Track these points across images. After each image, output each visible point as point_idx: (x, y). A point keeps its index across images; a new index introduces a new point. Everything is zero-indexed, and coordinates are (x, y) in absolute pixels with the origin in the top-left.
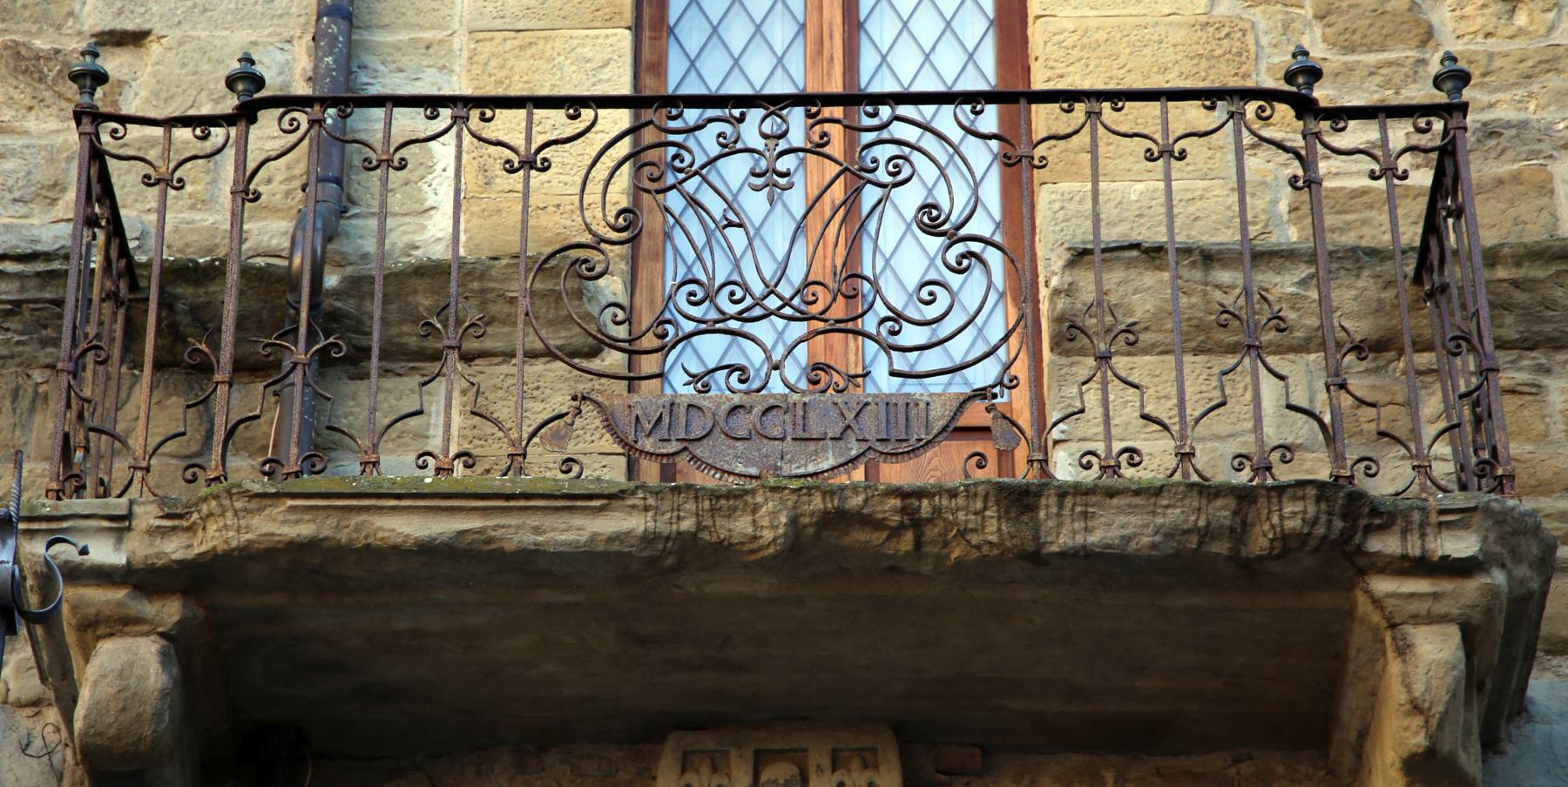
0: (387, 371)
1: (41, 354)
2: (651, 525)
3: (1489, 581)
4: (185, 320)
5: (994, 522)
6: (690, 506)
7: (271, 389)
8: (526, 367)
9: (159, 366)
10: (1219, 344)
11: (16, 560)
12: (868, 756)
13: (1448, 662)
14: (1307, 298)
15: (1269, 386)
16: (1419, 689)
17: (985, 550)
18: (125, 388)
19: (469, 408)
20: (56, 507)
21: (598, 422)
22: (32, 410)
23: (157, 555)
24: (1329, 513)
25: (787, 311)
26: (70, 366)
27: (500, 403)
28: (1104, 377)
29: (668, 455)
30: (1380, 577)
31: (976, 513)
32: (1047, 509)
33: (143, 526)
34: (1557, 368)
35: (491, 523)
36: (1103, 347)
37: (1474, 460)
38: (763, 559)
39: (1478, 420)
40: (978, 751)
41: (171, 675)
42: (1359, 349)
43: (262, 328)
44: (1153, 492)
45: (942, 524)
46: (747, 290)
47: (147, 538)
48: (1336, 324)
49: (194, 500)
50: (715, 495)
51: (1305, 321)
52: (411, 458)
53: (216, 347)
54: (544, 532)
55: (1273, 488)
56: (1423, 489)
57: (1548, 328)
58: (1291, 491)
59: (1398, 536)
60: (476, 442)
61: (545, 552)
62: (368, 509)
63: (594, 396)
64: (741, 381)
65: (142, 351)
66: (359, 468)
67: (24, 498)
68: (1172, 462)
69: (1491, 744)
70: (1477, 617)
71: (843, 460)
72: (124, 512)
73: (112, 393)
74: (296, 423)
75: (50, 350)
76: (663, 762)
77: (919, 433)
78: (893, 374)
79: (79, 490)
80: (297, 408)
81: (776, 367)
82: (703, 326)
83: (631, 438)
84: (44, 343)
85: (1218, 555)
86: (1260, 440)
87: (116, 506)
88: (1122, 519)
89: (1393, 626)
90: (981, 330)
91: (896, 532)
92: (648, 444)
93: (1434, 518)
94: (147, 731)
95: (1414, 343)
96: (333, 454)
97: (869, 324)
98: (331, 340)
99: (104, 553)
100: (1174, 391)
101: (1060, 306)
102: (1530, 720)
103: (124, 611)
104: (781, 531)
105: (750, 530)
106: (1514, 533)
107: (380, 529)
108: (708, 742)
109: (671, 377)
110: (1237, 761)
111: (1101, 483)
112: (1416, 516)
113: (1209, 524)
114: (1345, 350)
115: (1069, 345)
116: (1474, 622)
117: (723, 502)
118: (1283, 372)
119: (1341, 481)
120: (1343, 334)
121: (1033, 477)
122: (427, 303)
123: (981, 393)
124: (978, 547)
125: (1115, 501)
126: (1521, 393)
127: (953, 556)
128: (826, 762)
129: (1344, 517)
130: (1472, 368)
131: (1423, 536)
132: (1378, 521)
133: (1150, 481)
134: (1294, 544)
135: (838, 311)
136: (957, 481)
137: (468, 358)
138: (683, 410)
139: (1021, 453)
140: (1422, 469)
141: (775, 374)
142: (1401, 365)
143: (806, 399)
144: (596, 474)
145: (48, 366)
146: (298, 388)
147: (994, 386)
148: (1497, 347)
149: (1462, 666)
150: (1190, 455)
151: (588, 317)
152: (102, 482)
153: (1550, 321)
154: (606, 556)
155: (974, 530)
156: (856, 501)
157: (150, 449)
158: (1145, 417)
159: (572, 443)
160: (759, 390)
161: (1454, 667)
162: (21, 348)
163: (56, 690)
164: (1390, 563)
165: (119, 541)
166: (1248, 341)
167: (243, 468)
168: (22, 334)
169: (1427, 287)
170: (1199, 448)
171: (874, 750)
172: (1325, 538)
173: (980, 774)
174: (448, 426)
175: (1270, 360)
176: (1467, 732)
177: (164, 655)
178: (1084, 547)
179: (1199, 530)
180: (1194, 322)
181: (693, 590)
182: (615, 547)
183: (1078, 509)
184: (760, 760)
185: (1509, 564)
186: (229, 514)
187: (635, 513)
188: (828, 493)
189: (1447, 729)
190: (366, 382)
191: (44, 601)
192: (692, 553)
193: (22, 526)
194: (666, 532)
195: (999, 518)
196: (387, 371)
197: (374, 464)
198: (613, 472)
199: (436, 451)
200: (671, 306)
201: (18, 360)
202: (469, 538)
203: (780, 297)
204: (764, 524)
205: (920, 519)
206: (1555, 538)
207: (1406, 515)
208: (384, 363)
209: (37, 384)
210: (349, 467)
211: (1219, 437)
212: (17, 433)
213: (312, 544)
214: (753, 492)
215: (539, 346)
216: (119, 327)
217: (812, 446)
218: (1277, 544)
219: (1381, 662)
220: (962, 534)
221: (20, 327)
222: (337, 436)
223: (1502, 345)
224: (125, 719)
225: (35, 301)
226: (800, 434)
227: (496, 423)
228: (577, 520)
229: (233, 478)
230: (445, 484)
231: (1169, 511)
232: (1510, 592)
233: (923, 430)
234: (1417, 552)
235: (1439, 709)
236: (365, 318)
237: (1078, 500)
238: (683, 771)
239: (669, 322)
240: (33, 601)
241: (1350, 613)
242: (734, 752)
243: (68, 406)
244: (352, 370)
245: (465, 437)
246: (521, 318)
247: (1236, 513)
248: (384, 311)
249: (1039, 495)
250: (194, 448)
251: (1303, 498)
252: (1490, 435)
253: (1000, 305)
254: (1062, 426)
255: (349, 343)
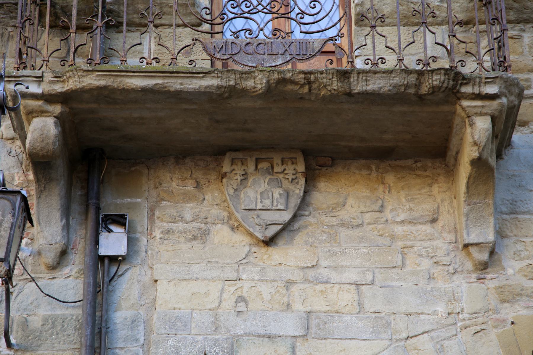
0: (129, 30)
1: (11, 22)
2: (220, 83)
3: (501, 101)
4: (59, 11)
5: (336, 82)
6: (233, 76)
7: (89, 35)
8: (176, 30)
9: (51, 27)
10: (412, 23)
11: (4, 90)
12: (294, 160)
13: (486, 129)
14: (442, 6)
15: (429, 35)
16: (476, 137)
17: (333, 92)
18: (39, 34)
19: (157, 43)
20: (17, 73)
21: (201, 49)
22: (8, 41)
23: (52, 90)
24: (449, 79)
25: (265, 10)
26: (21, 25)
27: (167, 42)
28: (373, 34)
29: (225, 59)
30: (465, 100)
31: (330, 80)
32: (353, 78)
33: (47, 80)
34: (527, 30)
35: (165, 81)
36: (373, 23)
37: (498, 61)
38: (258, 94)
39: (500, 47)
40: (330, 159)
41: (58, 130)
42: (460, 23)
43: (85, 14)
44: (390, 72)
45: (318, 83)
46: (251, 3)
47: (49, 84)
48: (453, 15)
49: (64, 72)
50: (241, 73)
51: (442, 15)
52: (138, 60)
53: (70, 21)
54: (183, 85)
55: (430, 71)
56: (480, 71)
57: (525, 16)
58: (436, 71)
59: (471, 87)
60: (160, 55)
61: (184, 91)
62: (124, 76)
63: (199, 39)
64: (250, 35)
65: (45, 22)
66: (120, 63)
67: (7, 70)
68: (395, 62)
69: (499, 156)
70: (496, 114)
71: (284, 61)
72: (41, 75)
73: (35, 36)
74: (98, 46)
75: (13, 20)
76: (225, 162)
77: (310, 52)
78: (301, 32)
79: (25, 67)
80: (98, 41)
81: (261, 30)
82: (237, 16)
83: (212, 53)
84: (12, 18)
85: (411, 93)
86: (426, 55)
87: (38, 73)
88: (379, 81)
89: (469, 117)
90: (331, 18)
91: (302, 86)
92: (218, 56)
93: (484, 80)
94: (51, 148)
95: (479, 22)
96: (111, 58)
97: (293, 15)
98: (110, 18)
99: (34, 89)
100: (397, 39)
101: (358, 10)
102: (512, 148)
103: (42, 109)
104: (264, 85)
105: (253, 85)
106: (510, 85)
107: (128, 83)
108: (240, 155)
109: (226, 34)
110: (416, 162)
111: (372, 69)
112: (478, 80)
113: (408, 83)
114: (455, 24)
115: (361, 23)
116: (496, 115)
117: (244, 75)
118: (435, 32)
119: (453, 68)
120: (455, 19)
121: (349, 67)
122: (142, 7)
123: (331, 39)
124: (330, 91)
125: (376, 75)
126: (515, 38)
127: (322, 94)
128: (280, 162)
129: (453, 80)
130: (498, 30)
131: (480, 86)
132: (465, 82)
133: (388, 69)
134: (436, 90)
135: (282, 11)
136: (322, 68)
137: (156, 26)
138: (230, 44)
139: (345, 60)
140: (480, 64)
141: (261, 32)
142: (474, 29)
143: (272, 41)
144: (201, 66)
145: (13, 26)
146: (99, 35)
147: (336, 37)
148: (508, 23)
149: (491, 130)
150: (402, 60)
151: (197, 12)
152: (33, 66)
153: (526, 13)
154: (205, 93)
155: (329, 85)
156: (289, 75)
157: (49, 55)
158: (387, 47)
159: (192, 56)
160: (256, 38)
161: (488, 130)
162: (3, 20)
163: (19, 134)
164: (468, 96)
165: (39, 85)
166: (422, 21)
167: (81, 62)
168: (4, 15)
169: (484, 2)
170: (405, 58)
171: (296, 158)
172: (447, 87)
173: (331, 166)
174: (150, 49)
175: (430, 28)
176: (492, 152)
177: (56, 123)
178: (366, 91)
179: (405, 85)
180: (404, 15)
181: (234, 105)
182: (208, 90)
183: (364, 78)
184: (258, 161)
185: (508, 95)
186: (76, 77)
187: (214, 79)
188: (280, 72)
189: (485, 150)
190: (121, 34)
191: (14, 104)
192: (234, 92)
193: (6, 79)
194: (225, 86)
195: (337, 81)
196: (129, 30)
197: (125, 61)
198: (207, 65)
199: (146, 57)
200: (225, 9)
201: (3, 24)
202: (158, 86)
203: (263, 6)
204: (258, 83)
205: (311, 81)
206: (524, 87)
207: (474, 79)
208: (128, 28)
209: (10, 32)
210: (116, 63)
211: (411, 55)
212: (3, 48)
213: (105, 88)
214: (254, 72)
215: (181, 22)
216: (37, 13)
217: (274, 57)
218: (430, 90)
219: (464, 129)
220: (325, 86)
221: (3, 12)
222: (112, 52)
223: (509, 22)
224: (43, 144)
225: (8, 3)
226: (270, 52)
227: (167, 48)
228: (195, 81)
229: (77, 65)
230: (149, 68)
231: (395, 79)
232: (508, 105)
233: (311, 51)
234: (478, 92)
235: (483, 144)
236: (121, 12)
237: (364, 75)
238: (232, 165)
239: (225, 14)
240: (10, 104)
241: (454, 113)
242: (249, 159)
243: (20, 39)
244: (117, 30)
245: (156, 53)
246: (174, 12)
247: (417, 79)
248: (127, 10)
249: (351, 73)
250: (64, 55)
251: (440, 74)
252: (504, 52)
253: (338, 10)
254: (358, 51)
255: (115, 20)
